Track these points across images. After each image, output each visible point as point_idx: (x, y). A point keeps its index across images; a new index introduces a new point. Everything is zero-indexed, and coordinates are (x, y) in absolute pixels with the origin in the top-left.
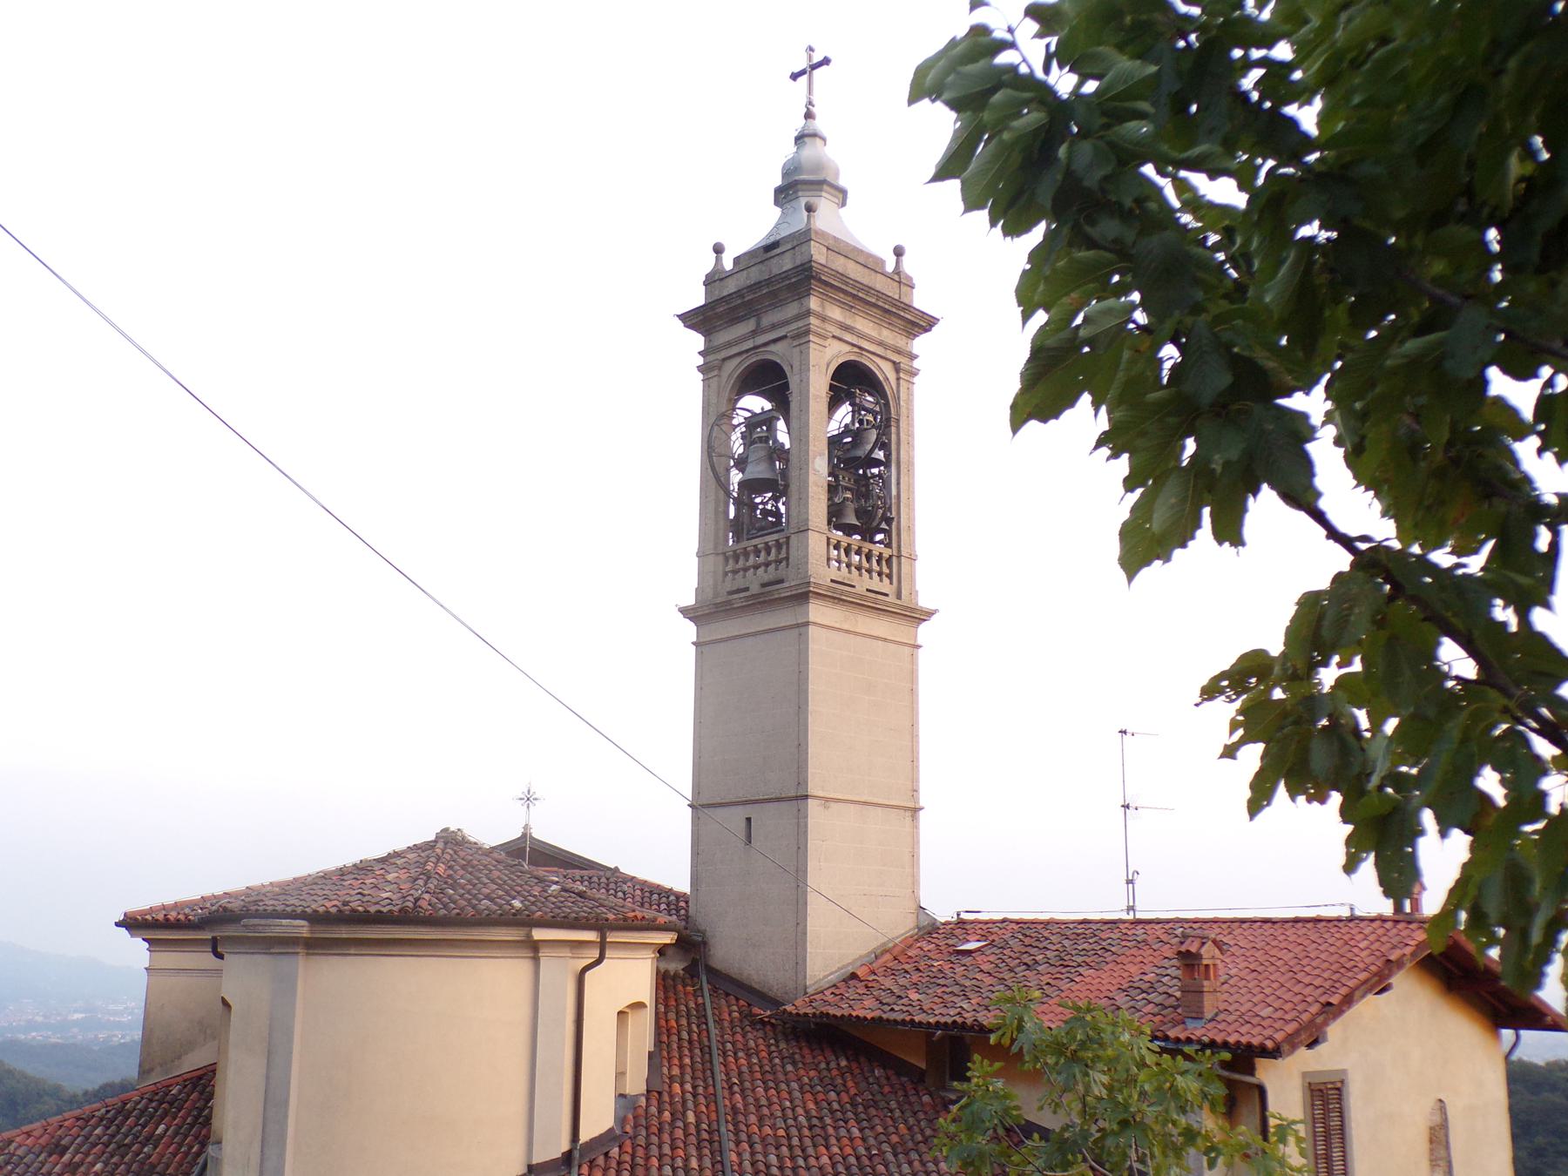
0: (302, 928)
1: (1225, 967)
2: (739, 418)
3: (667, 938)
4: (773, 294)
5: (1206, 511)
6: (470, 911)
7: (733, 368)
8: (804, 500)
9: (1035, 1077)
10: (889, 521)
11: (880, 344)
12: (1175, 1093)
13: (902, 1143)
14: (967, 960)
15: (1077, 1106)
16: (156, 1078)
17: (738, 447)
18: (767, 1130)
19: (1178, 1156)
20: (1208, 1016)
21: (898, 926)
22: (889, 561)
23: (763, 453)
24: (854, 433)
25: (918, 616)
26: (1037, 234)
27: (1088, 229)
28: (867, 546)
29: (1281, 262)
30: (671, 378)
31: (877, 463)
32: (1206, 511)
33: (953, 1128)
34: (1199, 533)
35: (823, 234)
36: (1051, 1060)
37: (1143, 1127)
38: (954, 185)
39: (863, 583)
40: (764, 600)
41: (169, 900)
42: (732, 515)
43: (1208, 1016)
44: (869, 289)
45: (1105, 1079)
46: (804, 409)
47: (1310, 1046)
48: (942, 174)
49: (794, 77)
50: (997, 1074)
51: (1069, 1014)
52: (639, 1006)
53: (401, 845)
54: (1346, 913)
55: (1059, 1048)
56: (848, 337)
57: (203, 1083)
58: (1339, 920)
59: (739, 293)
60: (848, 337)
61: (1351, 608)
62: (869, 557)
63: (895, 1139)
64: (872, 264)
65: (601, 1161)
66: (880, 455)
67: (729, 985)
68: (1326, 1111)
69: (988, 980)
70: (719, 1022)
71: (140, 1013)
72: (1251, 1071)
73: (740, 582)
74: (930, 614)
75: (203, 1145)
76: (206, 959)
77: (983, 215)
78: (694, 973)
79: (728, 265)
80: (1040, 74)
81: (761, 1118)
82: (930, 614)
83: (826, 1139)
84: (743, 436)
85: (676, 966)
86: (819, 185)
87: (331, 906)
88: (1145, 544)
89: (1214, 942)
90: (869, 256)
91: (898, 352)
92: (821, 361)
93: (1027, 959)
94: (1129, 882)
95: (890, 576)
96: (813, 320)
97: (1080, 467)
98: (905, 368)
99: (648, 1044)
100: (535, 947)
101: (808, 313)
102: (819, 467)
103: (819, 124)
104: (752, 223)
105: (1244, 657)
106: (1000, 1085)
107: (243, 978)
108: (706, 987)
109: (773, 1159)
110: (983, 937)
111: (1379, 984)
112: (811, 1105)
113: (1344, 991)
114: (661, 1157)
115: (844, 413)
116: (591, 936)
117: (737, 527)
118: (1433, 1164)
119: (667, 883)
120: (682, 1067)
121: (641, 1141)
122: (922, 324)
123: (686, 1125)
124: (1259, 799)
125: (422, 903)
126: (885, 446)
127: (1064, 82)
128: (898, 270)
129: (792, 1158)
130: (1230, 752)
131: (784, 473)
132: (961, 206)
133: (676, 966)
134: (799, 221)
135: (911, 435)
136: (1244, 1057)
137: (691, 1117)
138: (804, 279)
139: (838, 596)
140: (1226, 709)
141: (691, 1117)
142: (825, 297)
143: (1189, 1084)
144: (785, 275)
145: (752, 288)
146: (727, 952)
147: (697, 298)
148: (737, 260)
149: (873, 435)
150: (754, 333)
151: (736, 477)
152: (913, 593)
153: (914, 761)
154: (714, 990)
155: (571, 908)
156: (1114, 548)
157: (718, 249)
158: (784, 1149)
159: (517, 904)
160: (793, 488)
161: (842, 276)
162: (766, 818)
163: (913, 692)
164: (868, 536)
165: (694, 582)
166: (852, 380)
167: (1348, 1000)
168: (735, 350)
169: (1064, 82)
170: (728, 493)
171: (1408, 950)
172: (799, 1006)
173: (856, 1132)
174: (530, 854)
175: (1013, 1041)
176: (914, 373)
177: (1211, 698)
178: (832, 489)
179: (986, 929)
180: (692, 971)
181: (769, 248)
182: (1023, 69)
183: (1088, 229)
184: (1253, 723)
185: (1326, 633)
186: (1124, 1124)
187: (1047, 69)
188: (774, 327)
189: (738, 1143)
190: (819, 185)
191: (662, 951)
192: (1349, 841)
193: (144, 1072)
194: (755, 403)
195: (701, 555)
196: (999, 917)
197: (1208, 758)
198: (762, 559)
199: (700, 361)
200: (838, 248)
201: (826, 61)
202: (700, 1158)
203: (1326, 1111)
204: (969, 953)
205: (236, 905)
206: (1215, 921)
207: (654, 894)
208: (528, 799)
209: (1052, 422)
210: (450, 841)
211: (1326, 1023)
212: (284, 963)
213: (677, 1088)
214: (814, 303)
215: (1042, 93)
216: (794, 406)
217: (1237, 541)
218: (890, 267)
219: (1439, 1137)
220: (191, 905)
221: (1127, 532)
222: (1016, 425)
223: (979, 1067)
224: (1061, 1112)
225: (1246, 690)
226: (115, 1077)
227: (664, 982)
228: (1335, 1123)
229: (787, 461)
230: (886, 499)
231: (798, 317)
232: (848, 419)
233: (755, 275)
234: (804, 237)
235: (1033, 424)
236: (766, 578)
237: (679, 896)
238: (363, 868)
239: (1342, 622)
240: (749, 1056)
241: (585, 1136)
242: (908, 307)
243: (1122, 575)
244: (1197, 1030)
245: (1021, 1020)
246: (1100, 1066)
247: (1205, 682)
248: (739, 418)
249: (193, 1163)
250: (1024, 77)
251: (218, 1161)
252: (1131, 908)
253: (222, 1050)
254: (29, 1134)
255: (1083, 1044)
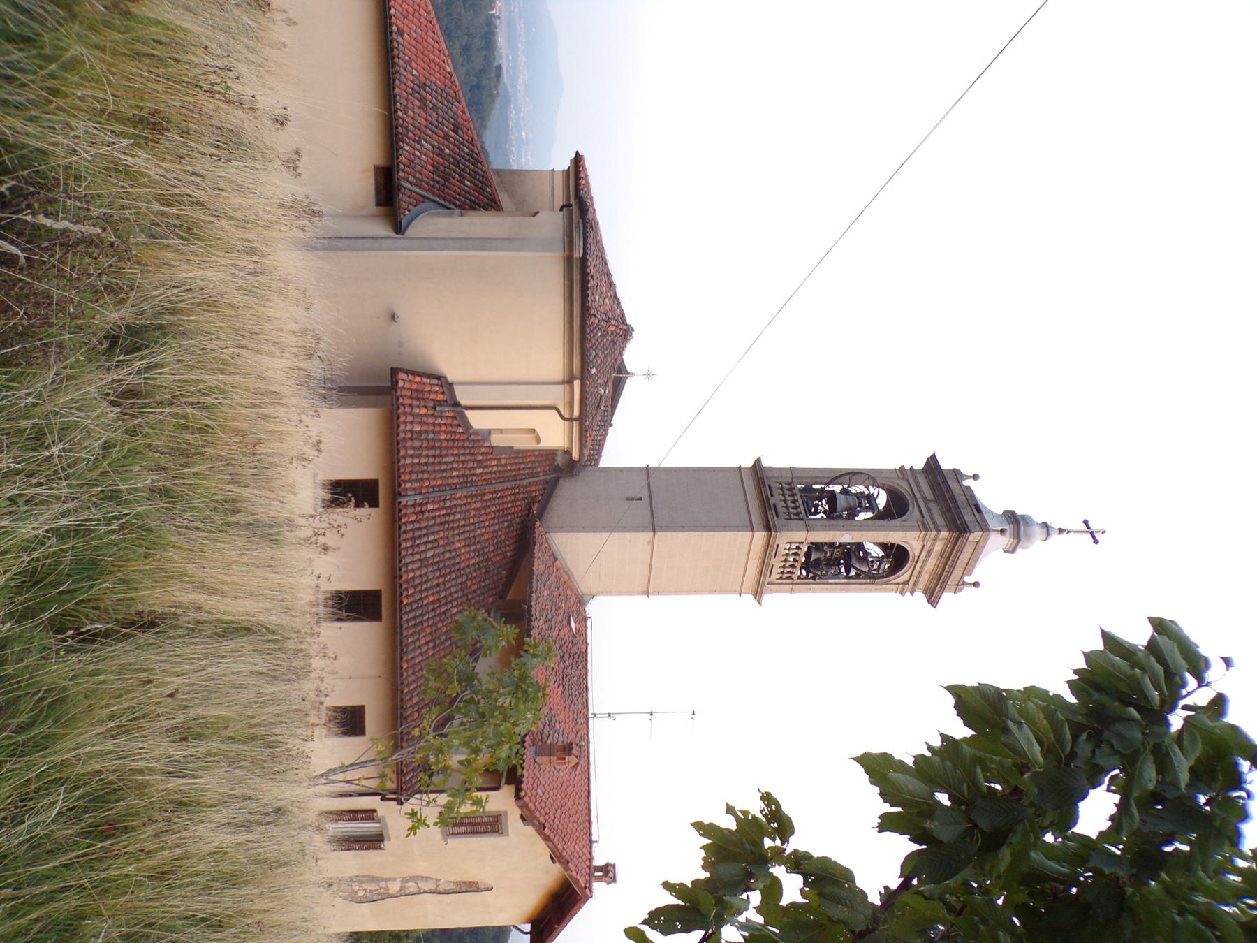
0: (578, 253)
1: (563, 770)
2: (873, 490)
3: (575, 455)
4: (949, 510)
5: (899, 809)
6: (589, 345)
7: (903, 487)
8: (825, 528)
9: (505, 663)
10: (814, 578)
11: (920, 573)
12: (500, 744)
13: (467, 588)
14: (565, 623)
15: (491, 687)
16: (495, 180)
17: (855, 489)
18: (473, 513)
19: (465, 744)
20: (538, 759)
21: (583, 588)
22: (790, 578)
23: (852, 504)
24: (865, 559)
25: (758, 594)
26: (1071, 699)
27: (1084, 736)
28: (798, 565)
29: (1058, 862)
30: (903, 453)
31: (848, 571)
32: (899, 809)
33: (480, 618)
34: (888, 805)
35: (986, 540)
36: (516, 673)
37: (482, 725)
38: (1099, 645)
39: (777, 563)
40: (766, 507)
41: (591, 179)
42: (815, 487)
43: (538, 759)
44: (953, 566)
45: (507, 704)
46: (880, 528)
47: (521, 816)
48: (1106, 636)
49: (1086, 522)
50: (508, 642)
51: (542, 682)
52: (538, 440)
53: (623, 306)
54: (594, 838)
55: (523, 678)
56: (924, 554)
57: (492, 204)
58: (590, 834)
59: (949, 490)
60: (924, 554)
61: (847, 906)
62: (792, 566)
63: (469, 583)
64: (968, 569)
65: (456, 422)
66: (853, 573)
67: (550, 489)
68: (486, 824)
69: (555, 634)
70: (530, 485)
71: (515, 167)
72: (508, 783)
73: (776, 492)
74: (759, 602)
75: (460, 207)
76: (559, 201)
77: (1082, 665)
78: (559, 470)
79: (966, 483)
80: (1182, 703)
81: (479, 509)
82: (759, 602)
83: (469, 546)
84: (862, 493)
85: (560, 460)
86: (1017, 537)
87: (591, 269)
88: (878, 768)
89: (577, 764)
90: (974, 567)
91: (915, 584)
92: (910, 539)
93: (566, 657)
94: (609, 715)
95: (781, 578)
96: (934, 533)
97: (922, 725)
98: (904, 588)
99: (517, 446)
100: (570, 382)
101: (938, 531)
102: (845, 537)
103: (1055, 537)
104: (993, 497)
105: (789, 820)
106: (503, 643)
107: (551, 223)
108: (548, 477)
109: (458, 516)
110: (578, 632)
111: (555, 857)
112: (486, 537)
113: (552, 836)
114: (458, 455)
115: (877, 552)
116: (576, 413)
117: (808, 489)
118: (458, 884)
119: (605, 453)
120: (506, 465)
121: (467, 444)
122: (933, 597)
123: (474, 468)
124: (700, 827)
125: (593, 319)
126: (858, 576)
127: (1176, 721)
128: (964, 584)
129: (458, 527)
130: (730, 810)
131: (840, 517)
132: (1087, 650)
133: (560, 460)
134: (994, 525)
135: (865, 591)
136: (514, 778)
137: (479, 471)
138: (959, 528)
139: (768, 547)
140: (756, 808)
141: (479, 471)
142: (948, 541)
143: (504, 751)
144: (960, 516)
145: (952, 496)
146: (568, 490)
147: (946, 464)
148: (969, 488)
149: (865, 569)
150: (925, 499)
151: (837, 488)
152: (771, 592)
153: (676, 592)
154: (546, 482)
155: (591, 401)
156: (876, 749)
157: (975, 477)
158: (462, 523)
159: (594, 371)
160: (832, 522)
161: (961, 551)
162: (641, 510)
163: (714, 592)
164: (805, 566)
165: (775, 465)
166: (897, 557)
167: (547, 839)
168: (914, 488)
169: (1176, 721)
170: (828, 484)
171: (574, 873)
172: (539, 529)
173: (472, 562)
174: (619, 377)
175: (526, 651)
176: (902, 593)
177: (762, 798)
178: (831, 545)
179: (582, 633)
180: (557, 469)
181: (978, 508)
182: (1184, 692)
183: (1084, 736)
184: (748, 825)
185: (829, 889)
186: (483, 715)
187: (1185, 708)
188: (929, 510)
189: (466, 497)
190: (1017, 537)
191: (568, 452)
192: (682, 885)
193: (498, 172)
194: (882, 500)
195: (791, 469)
196: (589, 641)
197: (729, 796)
198: (790, 504)
199: (907, 467)
200: (978, 548)
201: (1096, 542)
202: (458, 477)
203: (486, 824)
204: (569, 623)
205: (590, 216)
206: (588, 763)
207: (599, 445)
208: (649, 375)
209: (955, 711)
210: (626, 333)
211: (534, 825)
212: (559, 245)
213: (494, 463)
214: (944, 534)
215: (1170, 703)
216: (881, 522)
217: (882, 828)
218: (966, 579)
219: (472, 887)
220: (589, 191)
221: (886, 758)
222: (949, 688)
223: (511, 631)
224: (488, 678)
225: (769, 821)
226: (492, 157)
227: (551, 454)
228: (480, 829)
229: (848, 518)
230: (826, 576)
231: (935, 523)
232: (874, 554)
233: (961, 499)
234: (984, 528)
235: (952, 701)
236: (779, 507)
237: (597, 461)
238: (611, 286)
239: (836, 900)
240: (511, 502)
241: (468, 413)
242: (942, 590)
243: (858, 754)
244: (529, 753)
245: (538, 656)
246: (514, 701)
247: (774, 795)
248: (873, 490)
249: (450, 202)
250: (1179, 692)
251: (451, 215)
252: (595, 715)
253: (511, 214)
254: (463, 112)
255: (525, 692)
